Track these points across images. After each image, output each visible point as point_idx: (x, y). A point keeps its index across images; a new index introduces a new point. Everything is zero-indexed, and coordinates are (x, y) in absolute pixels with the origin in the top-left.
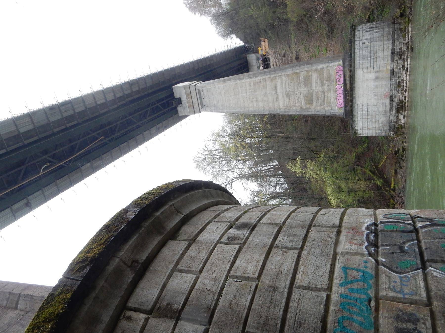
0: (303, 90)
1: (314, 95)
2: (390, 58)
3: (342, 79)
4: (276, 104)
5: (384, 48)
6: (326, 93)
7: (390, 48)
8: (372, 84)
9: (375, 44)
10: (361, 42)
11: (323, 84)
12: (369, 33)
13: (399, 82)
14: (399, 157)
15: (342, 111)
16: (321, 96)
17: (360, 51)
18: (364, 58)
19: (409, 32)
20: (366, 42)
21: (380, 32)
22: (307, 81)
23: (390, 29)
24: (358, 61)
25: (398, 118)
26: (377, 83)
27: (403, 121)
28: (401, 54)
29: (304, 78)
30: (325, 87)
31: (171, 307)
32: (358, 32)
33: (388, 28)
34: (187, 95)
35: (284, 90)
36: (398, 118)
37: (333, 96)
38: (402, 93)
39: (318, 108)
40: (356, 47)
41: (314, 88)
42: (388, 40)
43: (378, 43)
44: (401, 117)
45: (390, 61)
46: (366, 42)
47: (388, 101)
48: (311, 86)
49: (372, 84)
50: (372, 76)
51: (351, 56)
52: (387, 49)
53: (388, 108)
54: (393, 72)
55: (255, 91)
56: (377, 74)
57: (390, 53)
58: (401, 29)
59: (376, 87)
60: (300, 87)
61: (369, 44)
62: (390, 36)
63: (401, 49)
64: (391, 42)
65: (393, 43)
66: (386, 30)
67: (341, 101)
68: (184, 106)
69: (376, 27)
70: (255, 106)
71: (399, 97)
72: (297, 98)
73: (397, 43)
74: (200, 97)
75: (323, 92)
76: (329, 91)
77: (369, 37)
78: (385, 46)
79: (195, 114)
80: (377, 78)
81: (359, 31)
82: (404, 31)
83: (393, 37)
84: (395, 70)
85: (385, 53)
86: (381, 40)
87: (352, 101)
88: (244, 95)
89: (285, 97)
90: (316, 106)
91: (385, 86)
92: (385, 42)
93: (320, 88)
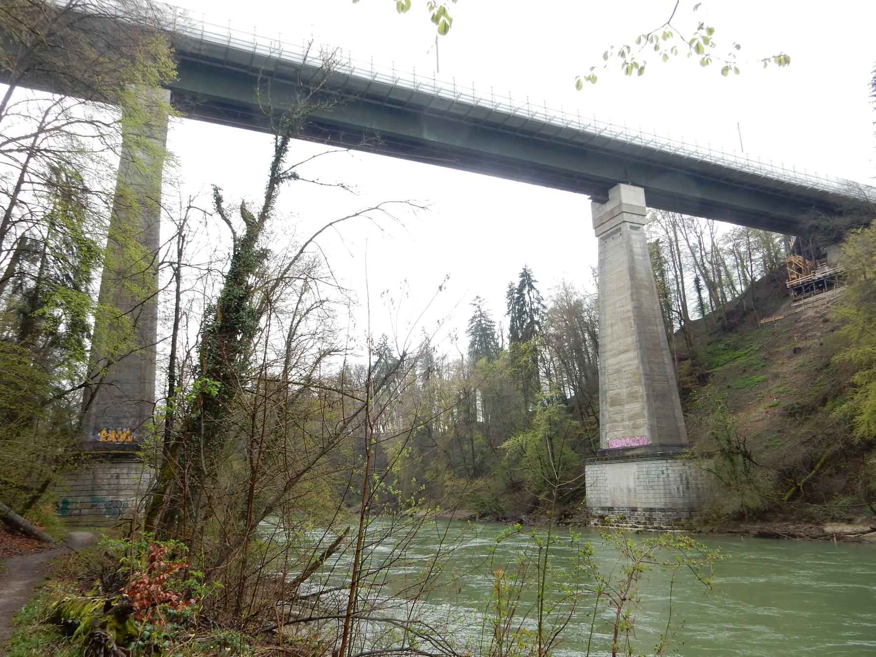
0: (624, 392)
1: (619, 408)
2: (648, 506)
3: (635, 444)
4: (610, 354)
5: (655, 500)
6: (621, 424)
7: (657, 506)
8: (624, 485)
9: (662, 488)
10: (664, 468)
11: (630, 418)
12: (678, 479)
13: (625, 518)
14: (564, 519)
15: (604, 447)
16: (618, 417)
17: (655, 467)
18: (648, 473)
19: (673, 529)
20: (664, 476)
21: (679, 492)
22: (632, 397)
23: (681, 506)
24: (646, 465)
25: (595, 517)
26: (625, 491)
27: (592, 523)
28: (650, 520)
29: (636, 392)
30: (627, 423)
31: (321, 385)
32: (681, 464)
33: (684, 504)
34: (612, 211)
35: (623, 364)
36: (595, 517)
37: (619, 433)
38: (615, 522)
39: (607, 414)
40: (660, 462)
41: (627, 407)
42: (666, 504)
43: (662, 491)
44: (595, 521)
45: (644, 506)
46: (664, 476)
47: (609, 505)
48: (628, 403)
49: (624, 485)
50: (632, 485)
51: (647, 456)
52: (656, 503)
53: (603, 505)
54: (634, 510)
55: (622, 320)
56: (633, 491)
57: (652, 506)
58: (680, 519)
59: (622, 490)
60: (627, 387)
61: (661, 480)
62: (670, 506)
63: (655, 519)
64: (663, 507)
65: (662, 510)
66: (681, 501)
67: (616, 444)
68: (601, 209)
69: (688, 488)
70: (608, 323)
71: (613, 518)
72: (615, 383)
73: (661, 514)
74: (613, 233)
75: (622, 420)
76: (624, 427)
77: (671, 479)
78: (658, 500)
79: (595, 228)
80: (629, 490)
81: (684, 465)
82: (676, 523)
83: (670, 510)
84: (636, 513)
85: (652, 501)
86: (665, 494)
87: (617, 459)
88: (618, 305)
89: (617, 367)
90: (609, 412)
91: (622, 501)
92: (663, 500)
93: (626, 415)
